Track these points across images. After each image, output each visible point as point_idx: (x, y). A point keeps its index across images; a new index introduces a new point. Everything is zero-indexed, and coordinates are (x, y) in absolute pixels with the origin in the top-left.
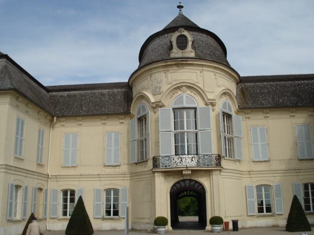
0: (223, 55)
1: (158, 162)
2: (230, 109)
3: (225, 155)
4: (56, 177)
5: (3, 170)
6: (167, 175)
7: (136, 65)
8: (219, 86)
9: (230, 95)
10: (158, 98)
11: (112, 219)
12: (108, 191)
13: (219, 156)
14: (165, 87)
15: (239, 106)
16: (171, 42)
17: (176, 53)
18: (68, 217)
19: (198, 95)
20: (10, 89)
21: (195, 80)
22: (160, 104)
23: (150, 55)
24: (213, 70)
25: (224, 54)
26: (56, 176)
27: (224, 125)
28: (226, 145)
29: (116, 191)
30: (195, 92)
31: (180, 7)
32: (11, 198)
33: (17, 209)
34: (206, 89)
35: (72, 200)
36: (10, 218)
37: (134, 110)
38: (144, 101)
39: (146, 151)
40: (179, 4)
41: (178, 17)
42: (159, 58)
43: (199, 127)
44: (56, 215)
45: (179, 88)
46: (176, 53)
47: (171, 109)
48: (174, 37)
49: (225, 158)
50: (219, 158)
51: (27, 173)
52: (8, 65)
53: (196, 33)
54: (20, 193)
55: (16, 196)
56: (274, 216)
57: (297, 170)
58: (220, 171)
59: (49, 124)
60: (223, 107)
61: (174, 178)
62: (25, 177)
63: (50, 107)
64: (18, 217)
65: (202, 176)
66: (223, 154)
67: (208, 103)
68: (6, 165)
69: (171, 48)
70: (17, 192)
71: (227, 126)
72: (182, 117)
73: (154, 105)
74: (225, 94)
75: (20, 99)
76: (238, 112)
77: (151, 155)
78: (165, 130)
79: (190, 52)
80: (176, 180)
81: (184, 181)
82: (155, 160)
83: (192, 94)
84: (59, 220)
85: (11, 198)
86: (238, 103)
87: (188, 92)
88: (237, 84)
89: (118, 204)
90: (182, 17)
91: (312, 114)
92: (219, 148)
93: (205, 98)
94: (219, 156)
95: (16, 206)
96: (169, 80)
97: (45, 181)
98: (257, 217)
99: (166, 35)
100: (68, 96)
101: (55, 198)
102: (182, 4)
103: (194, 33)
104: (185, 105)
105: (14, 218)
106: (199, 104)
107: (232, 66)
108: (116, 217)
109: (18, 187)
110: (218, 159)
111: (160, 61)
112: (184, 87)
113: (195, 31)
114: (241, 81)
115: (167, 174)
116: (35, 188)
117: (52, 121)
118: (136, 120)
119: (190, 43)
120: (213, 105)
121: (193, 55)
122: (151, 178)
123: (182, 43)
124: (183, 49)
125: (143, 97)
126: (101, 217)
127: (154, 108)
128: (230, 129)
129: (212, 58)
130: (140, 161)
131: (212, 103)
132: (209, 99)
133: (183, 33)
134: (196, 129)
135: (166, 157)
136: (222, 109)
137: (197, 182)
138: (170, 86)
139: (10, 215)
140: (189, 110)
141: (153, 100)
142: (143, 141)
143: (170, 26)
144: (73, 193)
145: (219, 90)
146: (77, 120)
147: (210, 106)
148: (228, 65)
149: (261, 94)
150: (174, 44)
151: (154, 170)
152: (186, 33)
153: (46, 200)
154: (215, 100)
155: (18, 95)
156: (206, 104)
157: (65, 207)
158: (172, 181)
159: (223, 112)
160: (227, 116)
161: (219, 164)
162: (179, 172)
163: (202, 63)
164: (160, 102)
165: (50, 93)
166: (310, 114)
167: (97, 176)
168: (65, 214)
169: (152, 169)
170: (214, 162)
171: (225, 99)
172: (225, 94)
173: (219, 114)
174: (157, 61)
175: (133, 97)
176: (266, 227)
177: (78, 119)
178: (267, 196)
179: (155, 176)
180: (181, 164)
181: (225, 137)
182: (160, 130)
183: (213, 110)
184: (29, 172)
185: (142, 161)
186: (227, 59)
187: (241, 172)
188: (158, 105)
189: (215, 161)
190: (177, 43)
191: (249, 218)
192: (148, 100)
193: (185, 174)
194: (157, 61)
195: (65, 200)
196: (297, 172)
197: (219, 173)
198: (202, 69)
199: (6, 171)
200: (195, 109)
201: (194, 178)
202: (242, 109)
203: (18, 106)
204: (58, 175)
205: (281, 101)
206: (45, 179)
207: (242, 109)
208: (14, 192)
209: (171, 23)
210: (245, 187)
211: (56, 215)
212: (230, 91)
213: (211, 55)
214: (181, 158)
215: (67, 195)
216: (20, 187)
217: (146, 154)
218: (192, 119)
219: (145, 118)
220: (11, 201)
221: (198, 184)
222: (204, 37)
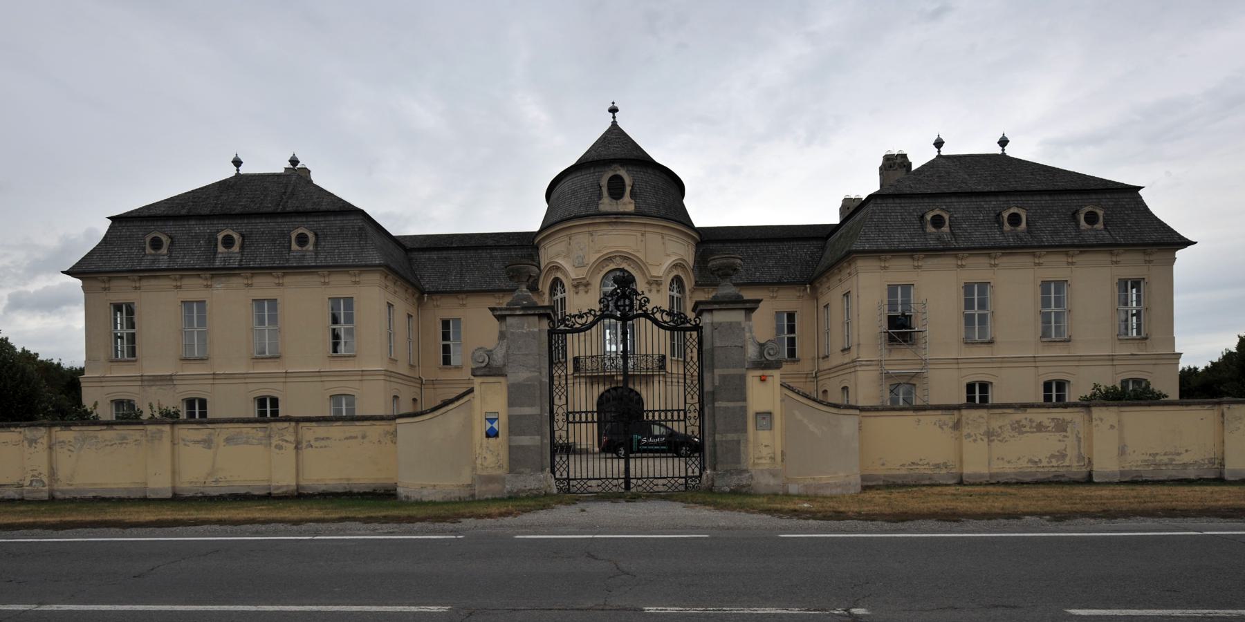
4: (433, 382)
5: (382, 377)
15: (696, 282)
20: (380, 265)
31: (613, 110)
46: (607, 204)
75: (389, 276)
79: (627, 204)
81: (615, 389)
86: (695, 276)
90: (615, 134)
93: (647, 274)
100: (438, 258)
112: (618, 258)
115: (593, 380)
119: (628, 189)
121: (631, 208)
122: (669, 384)
123: (616, 189)
132: (652, 277)
133: (618, 173)
141: (574, 277)
146: (458, 298)
147: (654, 286)
152: (622, 172)
155: (387, 272)
158: (598, 390)
161: (662, 366)
163: (644, 222)
186: (684, 201)
190: (609, 189)
212: (685, 260)
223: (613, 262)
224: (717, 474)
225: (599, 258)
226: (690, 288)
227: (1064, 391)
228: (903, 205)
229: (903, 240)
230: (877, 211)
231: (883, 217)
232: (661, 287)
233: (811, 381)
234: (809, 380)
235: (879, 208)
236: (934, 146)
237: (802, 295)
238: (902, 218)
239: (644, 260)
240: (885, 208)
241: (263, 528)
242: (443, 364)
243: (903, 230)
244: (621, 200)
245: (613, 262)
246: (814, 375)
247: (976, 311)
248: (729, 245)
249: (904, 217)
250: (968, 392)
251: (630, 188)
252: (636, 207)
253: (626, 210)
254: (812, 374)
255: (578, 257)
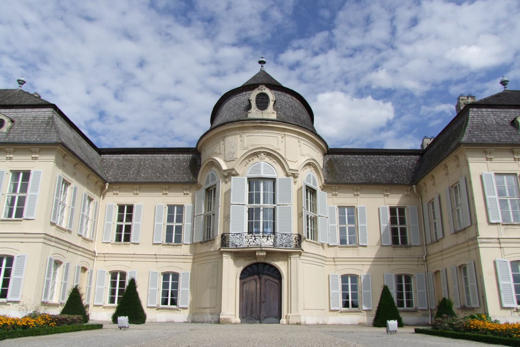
0: (309, 121)
1: (227, 240)
2: (315, 183)
3: (306, 236)
5: (42, 240)
6: (236, 257)
7: (207, 125)
8: (303, 155)
9: (315, 167)
10: (231, 165)
11: (169, 309)
12: (166, 276)
13: (300, 236)
14: (240, 153)
15: (325, 180)
16: (249, 101)
17: (255, 113)
18: (116, 304)
19: (278, 164)
20: (56, 144)
21: (276, 146)
22: (234, 172)
23: (224, 115)
24: (296, 136)
25: (310, 119)
26: (104, 254)
27: (307, 201)
28: (308, 225)
29: (176, 276)
30: (274, 160)
32: (49, 276)
33: (55, 290)
34: (287, 157)
35: (122, 284)
36: (45, 300)
37: (203, 178)
38: (214, 169)
39: (213, 227)
40: (261, 59)
41: (259, 73)
42: (235, 118)
43: (278, 202)
44: (101, 301)
45: (256, 154)
46: (255, 113)
47: (246, 179)
48: (253, 95)
49: (307, 239)
50: (300, 239)
51: (69, 247)
52: (55, 116)
53: (279, 93)
54: (60, 270)
55: (55, 273)
56: (361, 312)
57: (390, 259)
58: (300, 254)
59: (99, 191)
60: (307, 180)
61: (245, 261)
62: (68, 251)
63: (102, 172)
64: (56, 300)
65: (278, 260)
66: (305, 235)
67: (290, 174)
68: (45, 234)
69: (249, 107)
70: (55, 270)
71: (311, 203)
72: (258, 189)
73: (226, 174)
74: (309, 164)
76: (324, 188)
77: (220, 232)
78: (237, 203)
79: (270, 113)
80: (247, 263)
81: (257, 264)
82: (224, 238)
83: (271, 162)
84: (104, 307)
85: (49, 276)
86: (324, 177)
87: (267, 159)
88: (325, 155)
89: (177, 291)
90: (263, 74)
91: (409, 193)
92: (300, 227)
94: (300, 236)
95: (53, 287)
96: (246, 144)
97: (91, 259)
98: (341, 312)
99: (244, 93)
101: (101, 283)
102: (264, 60)
103: (277, 92)
104: (263, 175)
105: (50, 301)
106: (278, 173)
107: (318, 132)
108: (174, 307)
109: (58, 263)
110: (298, 240)
111: (235, 122)
112: (262, 154)
113: (278, 90)
114: (329, 152)
115: (237, 255)
116: (79, 267)
117: (103, 188)
118: (203, 192)
119: (271, 103)
120: (295, 176)
121: (274, 116)
124: (263, 110)
125: (214, 164)
126: (156, 306)
127: (226, 177)
128: (314, 208)
129: (296, 122)
130: (206, 239)
131: (294, 174)
132: (290, 170)
133: (264, 91)
134: (274, 203)
135: (237, 234)
136: (306, 182)
137: (272, 266)
138: (246, 151)
139: (46, 296)
140: (267, 181)
142: (210, 216)
143: (249, 83)
144: (123, 275)
145: (303, 160)
147: (292, 178)
148: (314, 132)
149: (351, 167)
150: (253, 103)
151: (222, 250)
152: (267, 91)
153: (90, 284)
154: (297, 171)
156: (287, 175)
157: (113, 292)
158: (245, 263)
159: (306, 186)
160: (311, 191)
161: (299, 245)
162: (253, 254)
164: (233, 169)
165: (102, 156)
166: (406, 193)
167: (154, 256)
168: (112, 301)
169: (220, 249)
170: (294, 243)
171: (310, 171)
172: (309, 164)
173: (302, 187)
174: (232, 122)
175: (202, 163)
176: (351, 325)
177: (134, 187)
178: (354, 288)
179: (223, 257)
180: (254, 244)
181: (308, 216)
182: (232, 203)
183: (295, 182)
184: (72, 246)
185: (208, 239)
186: (314, 126)
187: (324, 258)
188: (230, 174)
189: (295, 241)
190: (257, 102)
191: (332, 313)
192: (218, 167)
193: (258, 256)
194: (232, 122)
195: (113, 284)
196: (389, 261)
197: (298, 256)
198: (284, 133)
199: (45, 241)
200: (274, 180)
201: (268, 261)
202: (328, 186)
203: (64, 166)
204: (107, 254)
205: (374, 177)
206: (90, 257)
207: (328, 186)
208: (53, 269)
209: (250, 80)
210: (329, 276)
211: (101, 301)
213: (296, 119)
214: (255, 237)
215: (116, 278)
216: (61, 263)
217: (213, 231)
218: (270, 192)
219: (215, 189)
220: (48, 279)
221: (274, 269)
222: (288, 97)
223: (258, 157)
224: (419, 107)
225: (245, 154)
226: (321, 185)
227: (411, 283)
228: (494, 113)
229: (503, 137)
230: (475, 116)
231: (481, 121)
232: (298, 179)
233: (422, 264)
234: (471, 248)
235: (477, 115)
236: (501, 85)
237: (409, 193)
238: (496, 122)
239: (284, 158)
240: (481, 115)
241: (139, 332)
242: (116, 241)
243: (500, 130)
244: (266, 110)
245: (258, 157)
246: (424, 259)
247: (347, 226)
248: (349, 156)
249: (497, 121)
250: (343, 282)
251: (273, 102)
252: (277, 116)
253: (270, 118)
254: (423, 258)
255: (229, 153)
